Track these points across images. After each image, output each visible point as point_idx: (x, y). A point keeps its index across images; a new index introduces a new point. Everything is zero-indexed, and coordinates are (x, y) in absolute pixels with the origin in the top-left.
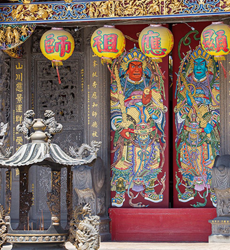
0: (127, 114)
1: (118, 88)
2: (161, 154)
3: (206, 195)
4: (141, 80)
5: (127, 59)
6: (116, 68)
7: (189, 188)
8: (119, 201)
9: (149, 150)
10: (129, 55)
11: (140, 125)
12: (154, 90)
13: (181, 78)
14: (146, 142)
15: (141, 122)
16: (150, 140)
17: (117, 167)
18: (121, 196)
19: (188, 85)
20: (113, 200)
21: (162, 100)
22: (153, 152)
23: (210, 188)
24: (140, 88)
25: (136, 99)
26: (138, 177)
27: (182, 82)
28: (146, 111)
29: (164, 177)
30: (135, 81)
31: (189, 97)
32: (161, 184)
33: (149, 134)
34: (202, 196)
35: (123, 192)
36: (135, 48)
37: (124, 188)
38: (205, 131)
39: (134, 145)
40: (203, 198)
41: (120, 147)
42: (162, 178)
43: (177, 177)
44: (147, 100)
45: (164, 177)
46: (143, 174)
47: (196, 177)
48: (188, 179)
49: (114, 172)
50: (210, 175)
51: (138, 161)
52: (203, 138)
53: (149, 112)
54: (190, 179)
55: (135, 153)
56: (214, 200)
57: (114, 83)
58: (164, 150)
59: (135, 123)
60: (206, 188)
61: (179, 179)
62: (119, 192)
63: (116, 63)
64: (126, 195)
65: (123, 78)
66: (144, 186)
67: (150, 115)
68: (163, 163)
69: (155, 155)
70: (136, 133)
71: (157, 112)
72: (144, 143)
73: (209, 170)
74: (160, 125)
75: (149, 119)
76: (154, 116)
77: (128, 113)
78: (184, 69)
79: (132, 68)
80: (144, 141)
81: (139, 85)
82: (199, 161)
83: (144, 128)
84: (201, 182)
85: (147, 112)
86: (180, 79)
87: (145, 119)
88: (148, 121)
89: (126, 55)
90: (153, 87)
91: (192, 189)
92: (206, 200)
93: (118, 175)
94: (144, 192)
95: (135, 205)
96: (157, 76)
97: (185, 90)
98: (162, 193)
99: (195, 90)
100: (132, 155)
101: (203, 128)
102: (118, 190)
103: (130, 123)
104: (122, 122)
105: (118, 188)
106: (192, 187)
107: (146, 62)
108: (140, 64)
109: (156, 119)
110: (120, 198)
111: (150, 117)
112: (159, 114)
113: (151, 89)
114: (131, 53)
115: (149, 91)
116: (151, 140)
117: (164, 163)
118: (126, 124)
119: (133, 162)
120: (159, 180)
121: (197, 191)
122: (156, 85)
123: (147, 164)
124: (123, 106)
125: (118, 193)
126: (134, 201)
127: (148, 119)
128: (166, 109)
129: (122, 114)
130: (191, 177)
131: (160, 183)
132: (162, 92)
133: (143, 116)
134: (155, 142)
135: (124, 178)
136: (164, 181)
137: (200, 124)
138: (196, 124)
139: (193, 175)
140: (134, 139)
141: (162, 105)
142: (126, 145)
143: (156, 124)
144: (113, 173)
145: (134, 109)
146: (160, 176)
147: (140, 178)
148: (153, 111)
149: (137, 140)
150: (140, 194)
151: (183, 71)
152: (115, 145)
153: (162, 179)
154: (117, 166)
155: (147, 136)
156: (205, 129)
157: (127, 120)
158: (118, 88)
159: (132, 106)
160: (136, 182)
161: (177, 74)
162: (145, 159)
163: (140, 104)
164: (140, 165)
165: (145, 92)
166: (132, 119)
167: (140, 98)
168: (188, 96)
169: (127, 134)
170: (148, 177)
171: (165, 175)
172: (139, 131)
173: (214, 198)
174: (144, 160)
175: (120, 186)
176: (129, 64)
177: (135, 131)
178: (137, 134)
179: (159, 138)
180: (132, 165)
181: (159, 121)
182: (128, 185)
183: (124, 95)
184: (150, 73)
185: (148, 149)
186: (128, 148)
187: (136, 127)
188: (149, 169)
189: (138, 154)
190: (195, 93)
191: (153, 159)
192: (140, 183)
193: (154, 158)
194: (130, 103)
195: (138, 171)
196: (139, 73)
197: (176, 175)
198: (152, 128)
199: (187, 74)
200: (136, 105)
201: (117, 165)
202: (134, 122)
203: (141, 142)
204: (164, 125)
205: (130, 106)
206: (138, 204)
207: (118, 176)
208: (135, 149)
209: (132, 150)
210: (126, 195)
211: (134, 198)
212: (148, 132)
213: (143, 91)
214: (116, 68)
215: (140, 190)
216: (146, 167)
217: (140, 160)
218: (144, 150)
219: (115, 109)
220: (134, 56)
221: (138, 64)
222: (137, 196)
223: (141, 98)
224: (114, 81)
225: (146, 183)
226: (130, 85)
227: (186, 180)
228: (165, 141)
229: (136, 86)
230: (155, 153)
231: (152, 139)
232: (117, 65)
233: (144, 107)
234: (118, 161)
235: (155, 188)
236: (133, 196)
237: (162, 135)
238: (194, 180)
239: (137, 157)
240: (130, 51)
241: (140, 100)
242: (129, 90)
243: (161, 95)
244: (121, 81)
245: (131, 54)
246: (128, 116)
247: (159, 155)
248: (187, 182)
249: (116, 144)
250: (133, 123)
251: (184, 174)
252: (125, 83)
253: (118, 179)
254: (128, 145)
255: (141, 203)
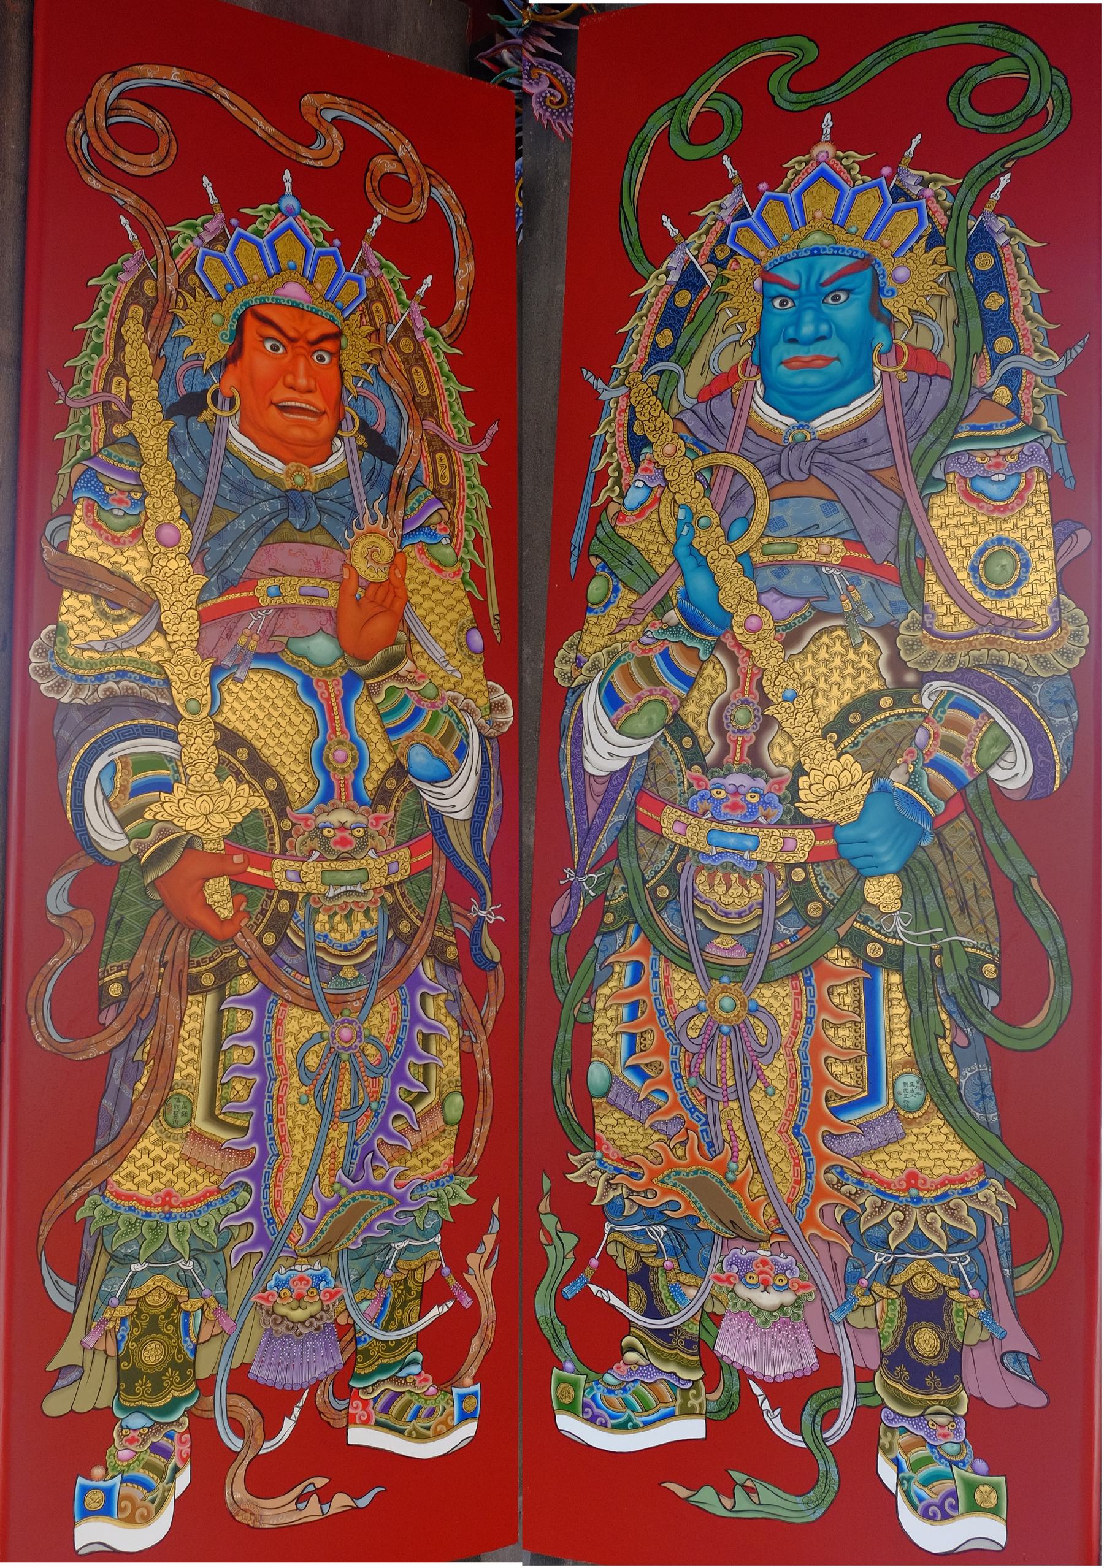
0: (218, 727)
1: (146, 494)
2: (467, 1060)
3: (830, 1418)
4: (334, 462)
5: (225, 277)
6: (133, 330)
7: (663, 1335)
8: (138, 1492)
9: (386, 1028)
10: (244, 246)
11: (323, 818)
12: (421, 551)
13: (632, 409)
14: (358, 967)
15: (328, 796)
16: (389, 944)
17: (129, 1186)
18: (155, 1448)
19: (701, 463)
20: (85, 1490)
21: (477, 639)
22: (411, 1042)
23: (873, 1362)
24: (325, 520)
25: (294, 608)
26: (297, 1257)
27: (637, 444)
28: (364, 712)
29: (489, 1240)
30: (285, 463)
31: (702, 562)
32: (467, 1302)
33: (389, 898)
34: (793, 1423)
35: (175, 1404)
36: (289, 201)
37: (184, 1368)
38: (846, 850)
39: (267, 990)
40: (795, 1440)
41: (154, 1011)
42: (474, 1250)
43: (550, 1222)
44: (375, 629)
45: (489, 1240)
46: (341, 1229)
47: (741, 1251)
48: (658, 1253)
49: (100, 1232)
50: (884, 1245)
51: (299, 1120)
52: (826, 912)
53: (391, 723)
54: (674, 1252)
55: (280, 1062)
56: (916, 1488)
57: (114, 450)
58: (490, 1026)
59: (280, 800)
60: (829, 1362)
61: (570, 1240)
62: (139, 1410)
63: (138, 283)
64: (202, 1429)
65: (195, 425)
66: (345, 1331)
67: (392, 749)
68: (481, 1130)
69: (426, 1067)
70: (286, 886)
71: (441, 728)
72: (349, 974)
73: (869, 1201)
74: (465, 832)
75: (384, 778)
76: (419, 758)
77: (231, 718)
78: (665, 339)
79: (264, 356)
80: (348, 951)
81: (316, 496)
82: (771, 1111)
83: (348, 846)
84: (788, 1297)
85: (374, 720)
86: (624, 418)
87: (357, 772)
88: (383, 796)
89: (220, 238)
90: (413, 531)
91: (689, 1344)
92: (828, 1466)
93: (136, 1259)
94: (342, 1384)
95: (277, 1512)
96: (444, 447)
97: (666, 507)
98: (473, 1371)
99: (763, 504)
100: (257, 1077)
101: (824, 828)
102: (130, 1391)
103: (243, 800)
104: (179, 790)
105: (128, 1378)
106: (694, 1329)
107: (369, 329)
108: (324, 338)
109: (432, 782)
110: (148, 1466)
111: (390, 759)
112: (454, 744)
113: (402, 538)
114: (259, 233)
115: (387, 553)
116: (398, 949)
117: (486, 1127)
118: (207, 808)
119: (259, 1137)
120: (453, 1271)
121: (744, 1376)
122: (435, 514)
123: (368, 1149)
124: (187, 652)
125: (137, 1421)
126: (268, 1478)
127: (376, 776)
128: (500, 706)
129: (178, 719)
130: (686, 1243)
131: (458, 1291)
132: (478, 575)
133: (340, 754)
134: (428, 964)
135: (188, 1282)
136: (489, 1273)
137: (794, 789)
138: (760, 783)
139: (709, 1223)
140: (269, 939)
141: (479, 673)
142: (205, 990)
143: (437, 817)
144: (87, 1248)
145: (278, 683)
146: (459, 1234)
147: (318, 1267)
148: (417, 713)
149: (297, 949)
150: (311, 1407)
151: (657, 354)
152: (115, 990)
153: (472, 1259)
154: (131, 1176)
155: (374, 915)
156: (842, 834)
157: (221, 779)
158: (146, 494)
159: (258, 656)
160: (283, 1310)
161: (600, 384)
162: (355, 1108)
163: (322, 647)
164: (318, 1155)
165: (361, 565)
166: (259, 769)
167: (323, 603)
168: (694, 552)
169: (218, 893)
170: (374, 1254)
171: (495, 1226)
172: (312, 870)
173: (915, 1466)
174: (345, 1115)
175: (152, 1354)
176: (241, 320)
177: (280, 873)
178: (291, 896)
179: (457, 932)
180: (248, 1155)
181: (456, 798)
182: (216, 1344)
183: (197, 557)
184: (393, 420)
185: (382, 1019)
186: (219, 1013)
187: (285, 835)
188: (385, 1188)
189: (301, 1062)
190: (756, 529)
191: (413, 1104)
192: (314, 1309)
193: (422, 1096)
194: (248, 637)
195: (298, 1209)
196: (316, 401)
197: (544, 1206)
198: (405, 852)
199: (694, 381)
200: (287, 657)
201: (128, 1167)
202: (268, 794)
203: (318, 962)
204: (489, 831)
205: (244, 657)
206: (301, 1498)
207: (136, 1267)
208: (279, 1022)
209: (256, 1036)
210: (202, 1429)
211: (268, 1447)
212: (378, 879)
213: (345, 548)
214: (133, 330)
215: (318, 1371)
216: (361, 1166)
217: (314, 1114)
218: (346, 1033)
219: (122, 675)
220: (284, 262)
221: (313, 335)
222: (288, 1425)
223: (332, 602)
224: (118, 430)
225: (362, 1312)
226: (244, 485)
227: (639, 1258)
228: (497, 958)
229: (292, 499)
230: (426, 1048)
231: (406, 941)
232: (150, 307)
233: (351, 681)
234: (139, 1133)
235: (423, 1339)
236: (259, 1433)
237: (476, 911)
238: (712, 1271)
239: (295, 1090)
240: (253, 219)
241: (324, 618)
242: (241, 525)
243: (469, 594)
244: (172, 439)
245: (263, 242)
246: (229, 740)
247: (453, 1067)
248: (643, 1276)
249: (124, 981)
250: (265, 804)
251: (616, 1206)
252: (206, 461)
253: (135, 1294)
254: (220, 988)
255: (320, 1482)
